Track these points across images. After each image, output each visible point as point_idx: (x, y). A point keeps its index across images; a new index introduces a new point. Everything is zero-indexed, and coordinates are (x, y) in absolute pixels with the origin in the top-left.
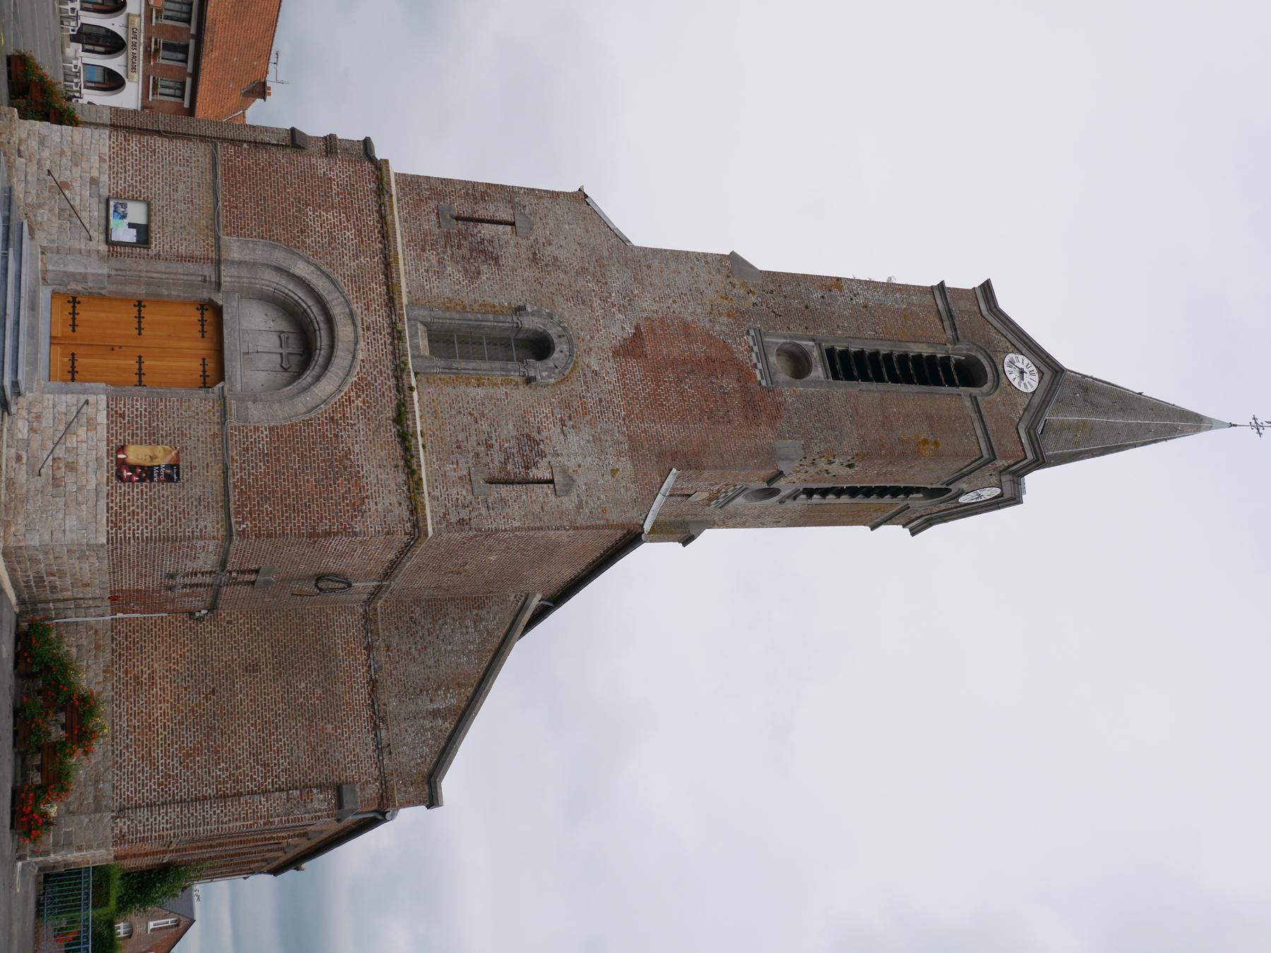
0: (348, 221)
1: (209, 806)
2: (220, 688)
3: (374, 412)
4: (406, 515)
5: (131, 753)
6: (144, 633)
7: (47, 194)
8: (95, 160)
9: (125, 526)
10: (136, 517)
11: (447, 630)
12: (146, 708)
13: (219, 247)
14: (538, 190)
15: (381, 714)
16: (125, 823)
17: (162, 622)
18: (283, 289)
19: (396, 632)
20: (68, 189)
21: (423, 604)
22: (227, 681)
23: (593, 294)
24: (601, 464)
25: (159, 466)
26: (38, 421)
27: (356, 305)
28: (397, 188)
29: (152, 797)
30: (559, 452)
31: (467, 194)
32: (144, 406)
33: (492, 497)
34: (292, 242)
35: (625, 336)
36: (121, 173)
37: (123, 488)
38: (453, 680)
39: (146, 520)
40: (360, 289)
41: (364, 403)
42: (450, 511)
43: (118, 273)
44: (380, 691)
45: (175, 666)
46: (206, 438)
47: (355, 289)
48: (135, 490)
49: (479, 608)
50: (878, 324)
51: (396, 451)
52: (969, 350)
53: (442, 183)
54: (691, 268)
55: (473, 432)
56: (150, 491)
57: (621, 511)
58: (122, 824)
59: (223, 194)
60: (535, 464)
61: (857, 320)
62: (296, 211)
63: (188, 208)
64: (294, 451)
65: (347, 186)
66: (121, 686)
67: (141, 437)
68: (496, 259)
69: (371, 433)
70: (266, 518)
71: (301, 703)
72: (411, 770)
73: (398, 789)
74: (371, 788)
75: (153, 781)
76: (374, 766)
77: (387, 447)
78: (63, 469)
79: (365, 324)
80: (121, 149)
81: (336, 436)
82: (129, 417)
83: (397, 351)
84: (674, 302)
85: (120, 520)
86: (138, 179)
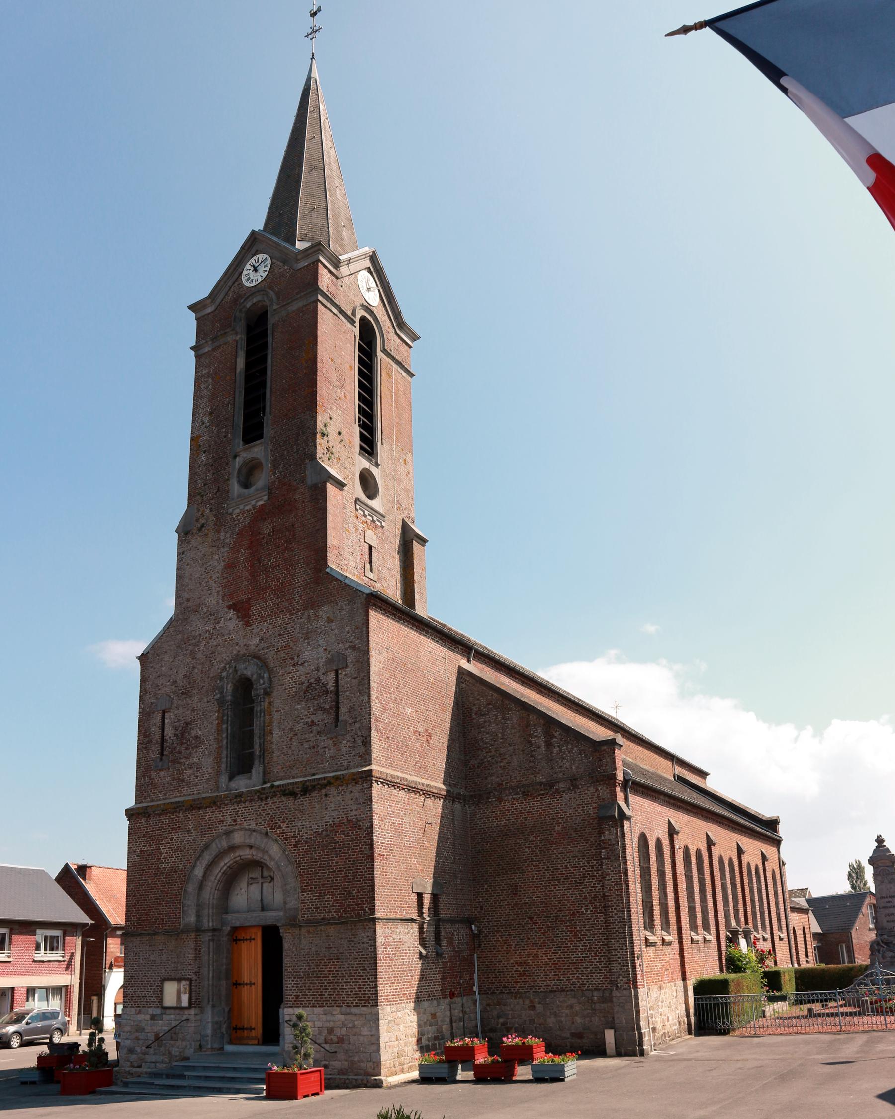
0: (167, 838)
1: (611, 919)
2: (528, 913)
6: (489, 971)
7: (162, 1049)
8: (141, 1017)
9: (368, 994)
10: (362, 986)
11: (487, 738)
12: (542, 967)
14: (140, 693)
16: (621, 980)
17: (481, 958)
18: (215, 884)
19: (489, 778)
20: (158, 1035)
21: (468, 758)
22: (523, 908)
29: (605, 961)
30: (316, 666)
32: (291, 982)
35: (235, 617)
37: (343, 996)
39: (364, 979)
40: (210, 828)
43: (211, 1000)
45: (512, 947)
46: (310, 938)
48: (345, 987)
49: (470, 713)
51: (316, 796)
53: (140, 768)
55: (303, 736)
56: (345, 976)
62: (162, 876)
63: (165, 953)
65: (144, 839)
66: (526, 986)
67: (311, 983)
68: (187, 724)
71: (539, 851)
72: (590, 762)
75: (593, 961)
78: (332, 1037)
79: (232, 823)
80: (132, 999)
82: (297, 992)
85: (364, 997)
86: (150, 988)
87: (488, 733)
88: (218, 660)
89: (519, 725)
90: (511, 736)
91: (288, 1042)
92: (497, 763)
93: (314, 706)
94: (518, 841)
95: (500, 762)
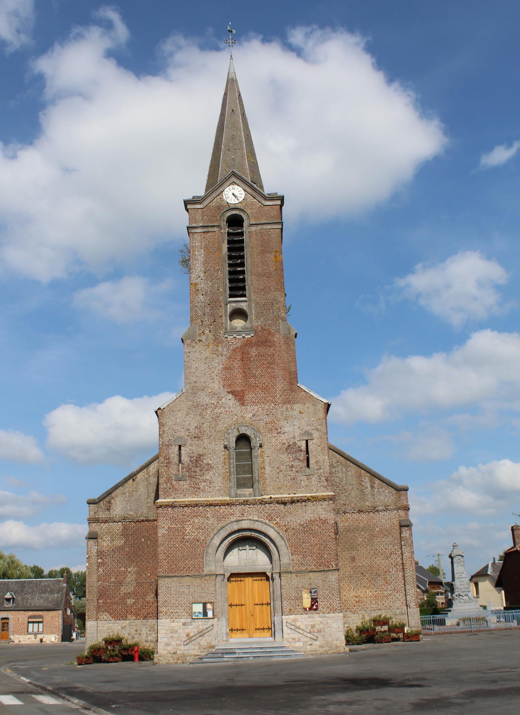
3: (282, 513)
4: (326, 503)
5: (385, 603)
11: (337, 480)
13: (210, 575)
15: (372, 509)
16: (412, 604)
23: (213, 412)
24: (297, 418)
25: (311, 596)
26: (295, 639)
27: (232, 519)
28: (168, 498)
30: (293, 436)
31: (166, 466)
32: (286, 602)
33: (315, 467)
34: (203, 545)
35: (233, 399)
36: (178, 614)
38: (358, 478)
41: (278, 518)
42: (323, 485)
44: (363, 509)
47: (224, 519)
48: (321, 604)
50: (214, 268)
52: (224, 221)
54: (194, 361)
55: (286, 473)
57: (319, 411)
58: (412, 605)
59: (183, 573)
60: (299, 447)
61: (213, 279)
63: (192, 587)
64: (301, 546)
69: (291, 515)
70: (330, 556)
72: (394, 498)
73: (402, 503)
74: (401, 514)
76: (392, 512)
77: (297, 509)
78: (314, 629)
79: (241, 516)
81: (293, 529)
83: (253, 503)
84: (213, 372)
86: (180, 607)
87: (337, 477)
88: (221, 422)
89: (356, 475)
90: (351, 480)
91: (285, 633)
92: (343, 493)
93: (293, 457)
94: (355, 534)
95: (345, 493)
